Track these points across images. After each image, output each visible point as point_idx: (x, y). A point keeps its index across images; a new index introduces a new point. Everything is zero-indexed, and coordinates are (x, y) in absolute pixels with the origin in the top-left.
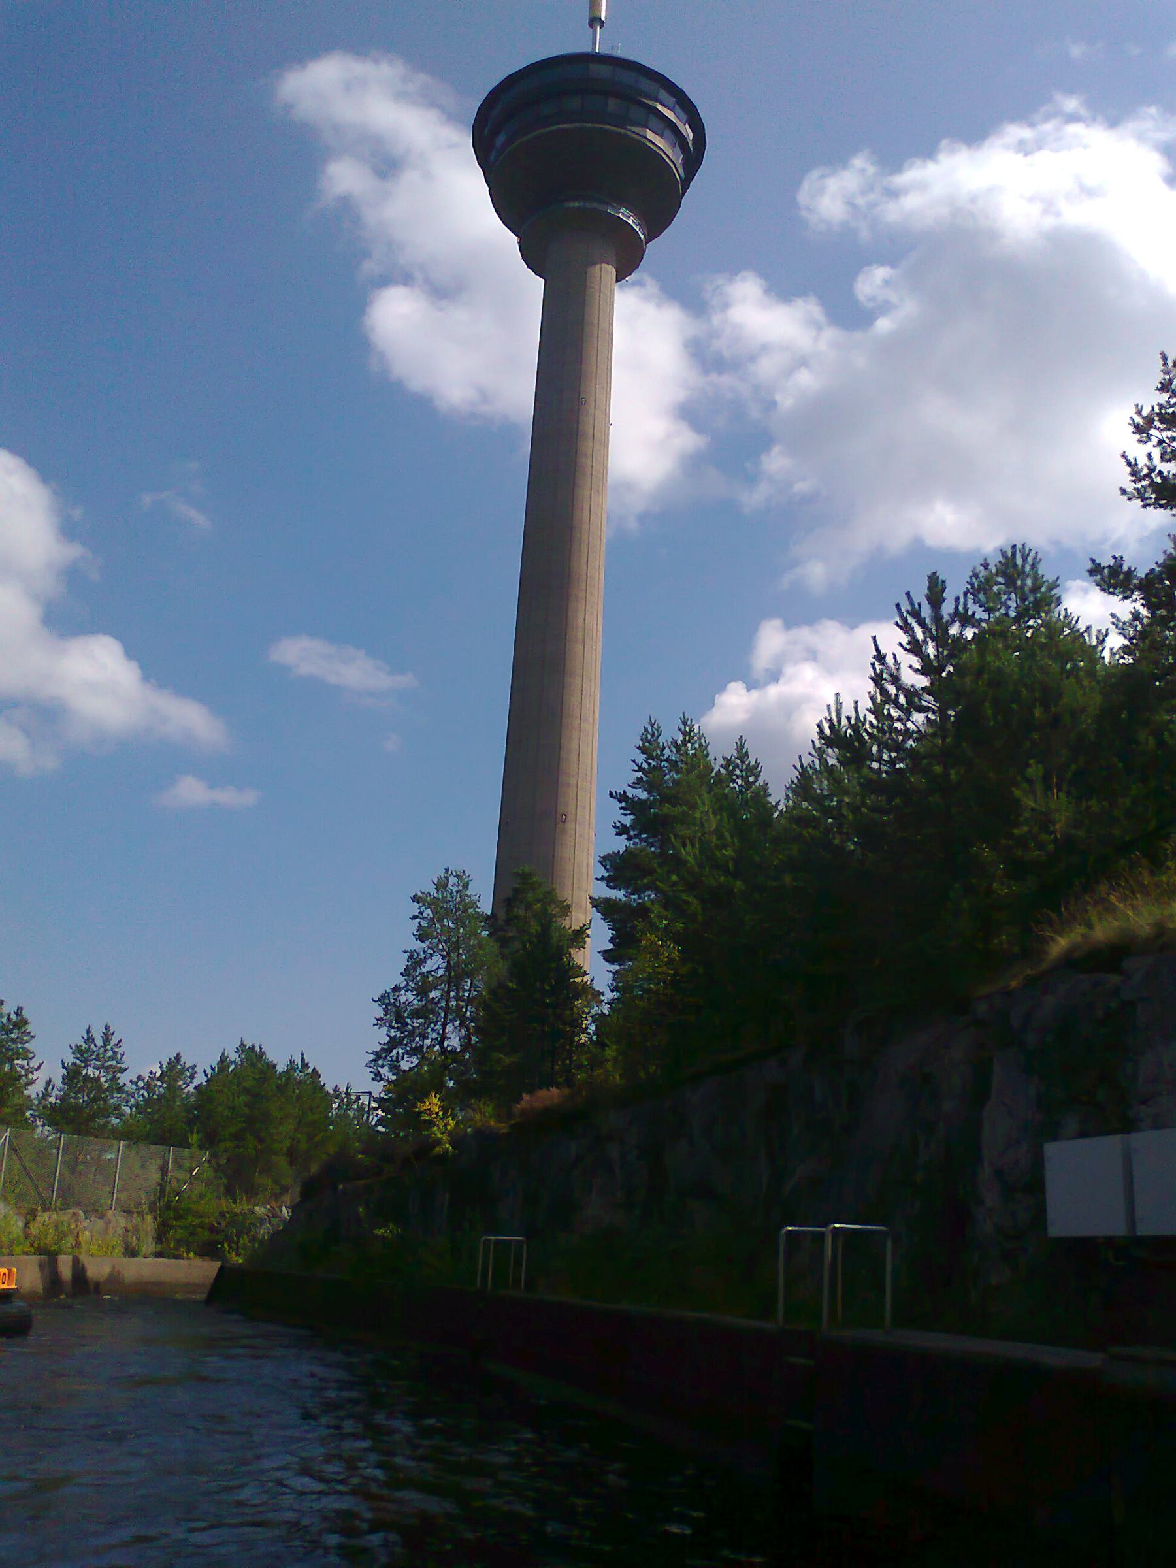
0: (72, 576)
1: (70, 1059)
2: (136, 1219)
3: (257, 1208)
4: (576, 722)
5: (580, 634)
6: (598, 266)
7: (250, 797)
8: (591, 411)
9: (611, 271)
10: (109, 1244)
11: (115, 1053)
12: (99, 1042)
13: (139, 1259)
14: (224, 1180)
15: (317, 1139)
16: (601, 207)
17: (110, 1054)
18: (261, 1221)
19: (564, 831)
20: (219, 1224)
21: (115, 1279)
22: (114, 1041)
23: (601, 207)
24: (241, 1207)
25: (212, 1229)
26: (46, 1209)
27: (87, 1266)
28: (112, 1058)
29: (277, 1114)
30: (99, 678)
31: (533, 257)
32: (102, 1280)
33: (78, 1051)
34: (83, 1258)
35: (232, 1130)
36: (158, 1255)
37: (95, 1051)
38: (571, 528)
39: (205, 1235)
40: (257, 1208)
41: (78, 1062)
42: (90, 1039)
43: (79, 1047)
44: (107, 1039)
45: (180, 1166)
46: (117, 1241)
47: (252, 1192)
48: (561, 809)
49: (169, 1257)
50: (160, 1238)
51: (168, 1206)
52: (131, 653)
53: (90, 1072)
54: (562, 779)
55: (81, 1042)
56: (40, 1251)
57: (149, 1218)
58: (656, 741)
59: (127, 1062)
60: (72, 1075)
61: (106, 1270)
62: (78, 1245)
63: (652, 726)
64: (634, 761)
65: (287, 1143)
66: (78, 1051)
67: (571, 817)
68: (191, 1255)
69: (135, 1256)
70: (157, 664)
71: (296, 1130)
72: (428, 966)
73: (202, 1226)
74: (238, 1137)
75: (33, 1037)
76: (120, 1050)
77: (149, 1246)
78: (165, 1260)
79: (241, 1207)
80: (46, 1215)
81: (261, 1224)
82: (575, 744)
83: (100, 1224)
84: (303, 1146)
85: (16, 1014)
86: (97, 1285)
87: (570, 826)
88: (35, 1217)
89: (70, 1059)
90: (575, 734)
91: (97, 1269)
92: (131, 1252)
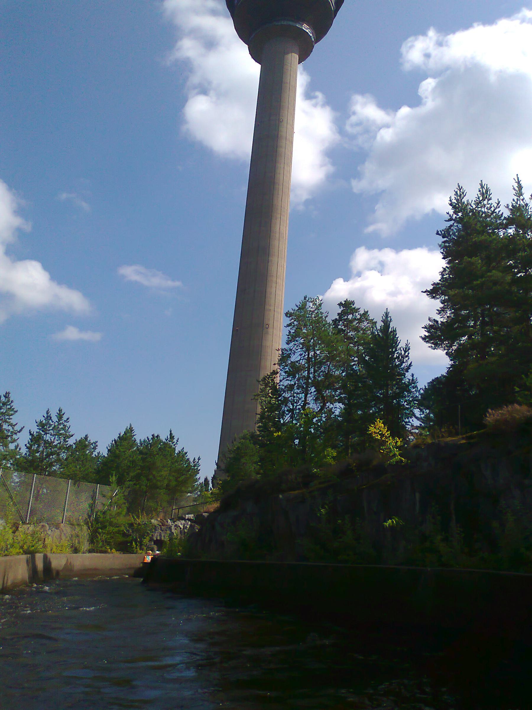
0: (19, 231)
1: (35, 430)
2: (78, 529)
3: (153, 521)
4: (274, 279)
5: (277, 235)
6: (290, 54)
7: (97, 336)
8: (285, 125)
9: (296, 57)
10: (66, 548)
11: (65, 426)
12: (55, 419)
13: (80, 554)
14: (127, 505)
15: (180, 479)
16: (294, 24)
17: (62, 426)
18: (155, 528)
19: (267, 333)
20: (128, 531)
21: (68, 568)
22: (65, 418)
23: (294, 24)
24: (142, 519)
25: (124, 535)
26: (24, 523)
27: (52, 560)
28: (63, 429)
29: (159, 464)
30: (31, 281)
31: (256, 55)
32: (61, 568)
33: (42, 425)
34: (49, 555)
35: (132, 474)
36: (90, 551)
37: (52, 425)
38: (274, 183)
39: (120, 539)
40: (153, 521)
41: (41, 431)
42: (49, 418)
43: (41, 422)
44: (60, 416)
45: (104, 496)
46: (65, 543)
47: (149, 512)
48: (266, 322)
49: (97, 552)
50: (92, 540)
51: (97, 520)
52: (45, 267)
53: (48, 437)
54: (267, 307)
55: (43, 419)
56: (25, 552)
57: (85, 528)
58: (461, 200)
59: (72, 431)
60: (35, 439)
61: (63, 562)
62: (45, 546)
63: (460, 190)
64: (448, 213)
65: (166, 482)
66: (42, 425)
67: (271, 326)
68: (114, 550)
69: (76, 553)
70: (58, 274)
71: (170, 474)
72: (294, 358)
73: (119, 532)
74: (137, 478)
75: (16, 412)
76: (68, 424)
77: (85, 546)
78: (99, 554)
79: (142, 519)
80: (25, 526)
81: (156, 530)
82: (273, 290)
83: (57, 532)
84: (174, 483)
85: (5, 397)
86: (58, 572)
87: (270, 330)
88: (17, 528)
89: (35, 430)
90: (274, 285)
91: (58, 562)
92: (76, 550)
